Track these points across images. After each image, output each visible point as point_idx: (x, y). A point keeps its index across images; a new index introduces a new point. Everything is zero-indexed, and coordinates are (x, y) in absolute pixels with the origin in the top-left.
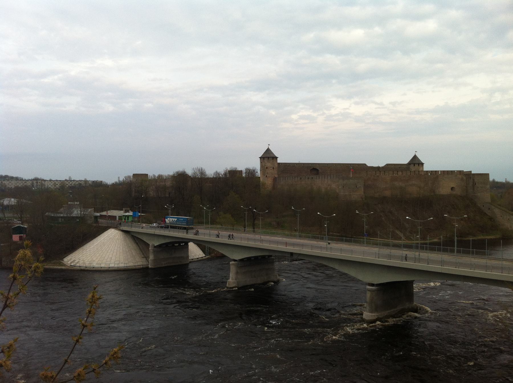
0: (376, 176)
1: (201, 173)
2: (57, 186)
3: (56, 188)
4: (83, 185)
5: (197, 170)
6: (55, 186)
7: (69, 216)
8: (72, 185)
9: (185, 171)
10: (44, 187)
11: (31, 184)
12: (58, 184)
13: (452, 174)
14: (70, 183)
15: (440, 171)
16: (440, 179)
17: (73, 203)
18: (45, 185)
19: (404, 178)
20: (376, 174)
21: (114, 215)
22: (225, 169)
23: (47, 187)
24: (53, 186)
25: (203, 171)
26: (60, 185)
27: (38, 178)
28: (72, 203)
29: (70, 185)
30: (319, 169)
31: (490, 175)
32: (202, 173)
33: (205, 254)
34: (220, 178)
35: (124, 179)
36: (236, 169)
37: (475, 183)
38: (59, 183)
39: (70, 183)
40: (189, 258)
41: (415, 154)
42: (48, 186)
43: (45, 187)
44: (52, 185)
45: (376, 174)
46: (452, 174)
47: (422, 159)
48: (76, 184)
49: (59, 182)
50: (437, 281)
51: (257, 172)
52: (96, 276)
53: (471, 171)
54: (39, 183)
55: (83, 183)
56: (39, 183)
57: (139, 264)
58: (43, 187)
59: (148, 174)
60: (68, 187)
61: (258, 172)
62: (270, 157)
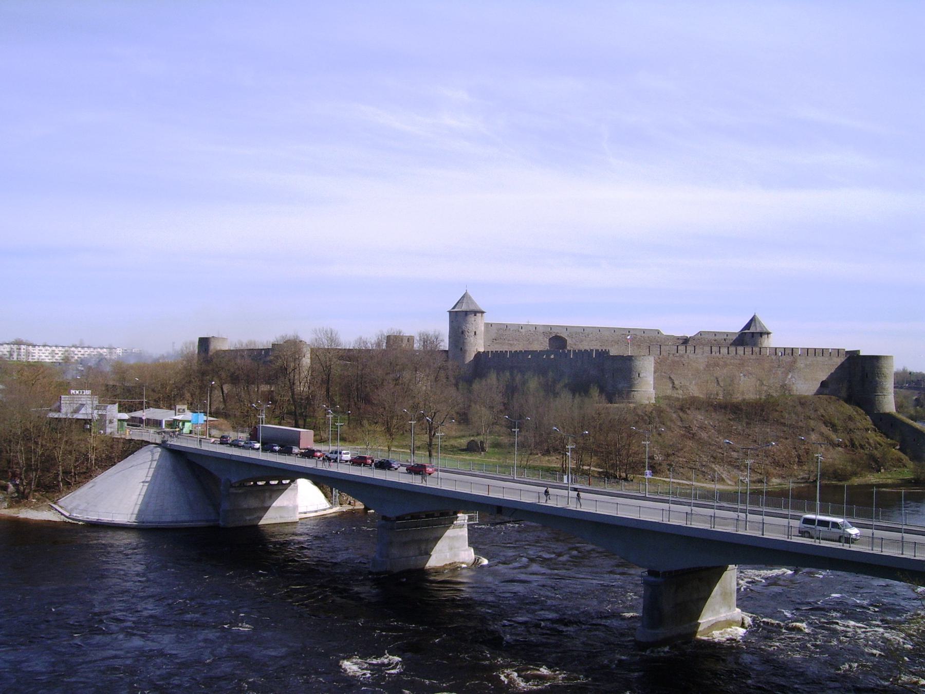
0: (678, 354)
1: (330, 338)
2: (57, 357)
3: (55, 361)
4: (106, 357)
5: (322, 334)
6: (53, 357)
7: (70, 417)
8: (86, 356)
9: (299, 335)
10: (32, 359)
11: (8, 352)
12: (58, 354)
13: (823, 355)
14: (80, 352)
15: (801, 348)
16: (799, 365)
17: (80, 392)
18: (34, 355)
19: (732, 361)
20: (677, 352)
21: (158, 418)
22: (379, 333)
23: (38, 359)
24: (50, 358)
25: (334, 335)
26: (62, 356)
27: (22, 341)
28: (77, 392)
29: (81, 356)
30: (566, 338)
31: (894, 358)
32: (365, 343)
33: (330, 501)
34: (368, 351)
35: (182, 347)
36: (400, 333)
37: (867, 374)
38: (60, 351)
39: (80, 352)
40: (299, 508)
41: (754, 314)
42: (40, 356)
43: (34, 359)
44: (47, 355)
45: (677, 352)
46: (823, 355)
47: (767, 323)
48: (93, 353)
49: (60, 348)
50: (776, 568)
51: (442, 341)
52: (108, 538)
53: (859, 351)
54: (24, 349)
55: (105, 352)
56: (24, 349)
57: (185, 517)
58: (30, 357)
59: (874, 361)
60: (77, 360)
61: (445, 341)
62: (470, 311)
